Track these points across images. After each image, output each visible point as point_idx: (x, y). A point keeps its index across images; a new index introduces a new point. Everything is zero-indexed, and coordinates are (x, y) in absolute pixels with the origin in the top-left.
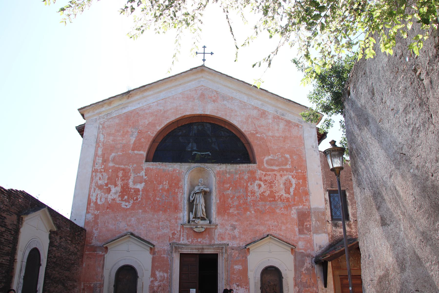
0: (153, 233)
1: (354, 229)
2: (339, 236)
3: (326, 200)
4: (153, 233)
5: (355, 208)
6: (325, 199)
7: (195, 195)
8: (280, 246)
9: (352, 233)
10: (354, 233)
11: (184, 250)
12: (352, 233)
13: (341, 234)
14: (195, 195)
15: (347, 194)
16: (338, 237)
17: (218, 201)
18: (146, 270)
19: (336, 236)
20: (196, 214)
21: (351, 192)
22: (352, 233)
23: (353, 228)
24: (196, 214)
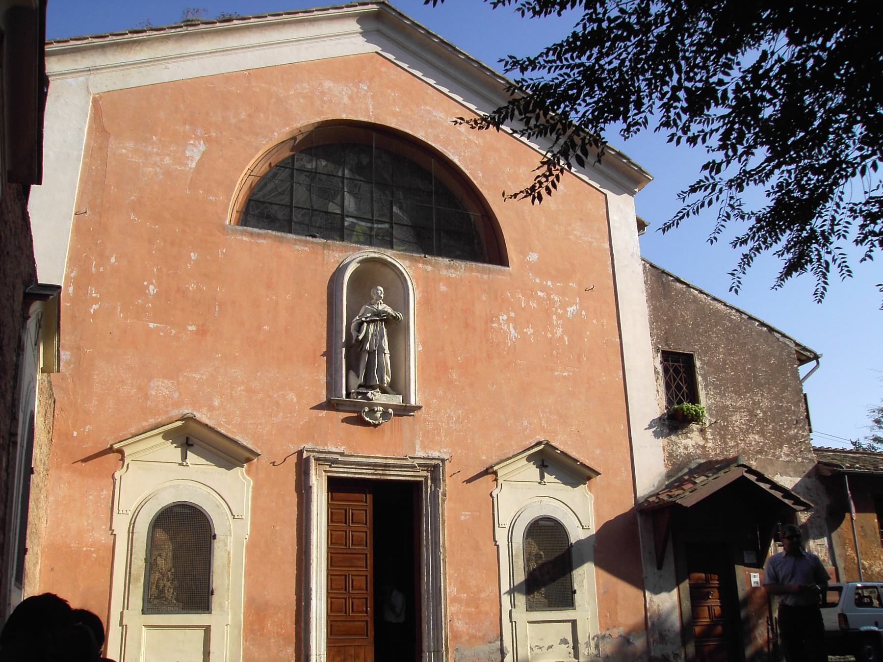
0: (703, 341)
1: (711, 441)
2: (682, 454)
3: (656, 372)
4: (703, 341)
5: (712, 395)
6: (655, 368)
7: (368, 325)
8: (135, 512)
9: (707, 450)
10: (710, 451)
11: (392, 473)
12: (708, 451)
13: (686, 452)
14: (368, 325)
15: (698, 364)
16: (681, 456)
17: (420, 348)
18: (585, 527)
19: (677, 455)
20: (368, 376)
21: (704, 360)
22: (708, 451)
23: (710, 439)
24: (368, 376)
